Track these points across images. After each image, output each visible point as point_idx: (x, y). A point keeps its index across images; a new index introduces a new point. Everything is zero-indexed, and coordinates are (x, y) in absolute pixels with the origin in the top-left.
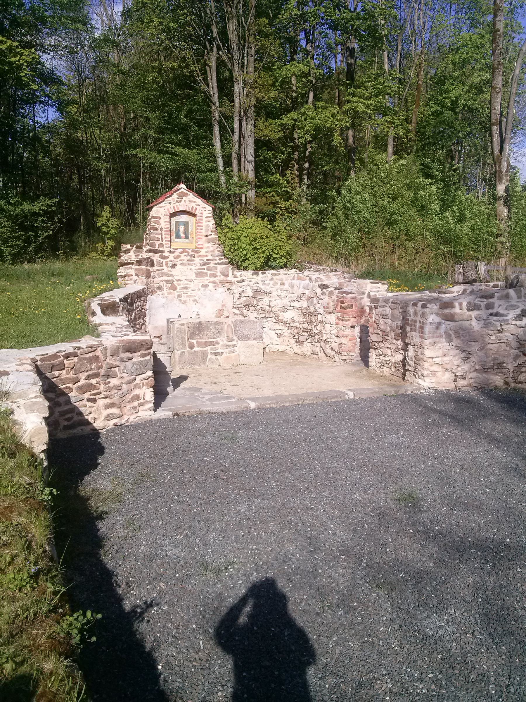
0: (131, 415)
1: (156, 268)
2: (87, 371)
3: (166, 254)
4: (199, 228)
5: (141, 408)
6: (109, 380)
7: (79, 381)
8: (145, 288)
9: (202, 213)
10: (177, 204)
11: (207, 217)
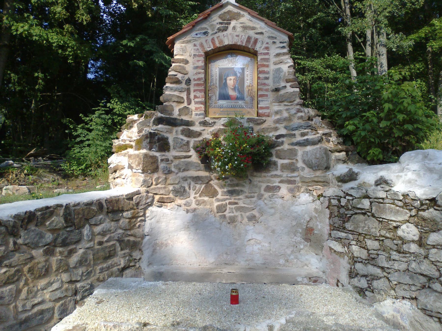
1: (173, 153)
3: (197, 128)
4: (261, 76)
8: (138, 193)
9: (267, 48)
10: (221, 34)
11: (278, 55)
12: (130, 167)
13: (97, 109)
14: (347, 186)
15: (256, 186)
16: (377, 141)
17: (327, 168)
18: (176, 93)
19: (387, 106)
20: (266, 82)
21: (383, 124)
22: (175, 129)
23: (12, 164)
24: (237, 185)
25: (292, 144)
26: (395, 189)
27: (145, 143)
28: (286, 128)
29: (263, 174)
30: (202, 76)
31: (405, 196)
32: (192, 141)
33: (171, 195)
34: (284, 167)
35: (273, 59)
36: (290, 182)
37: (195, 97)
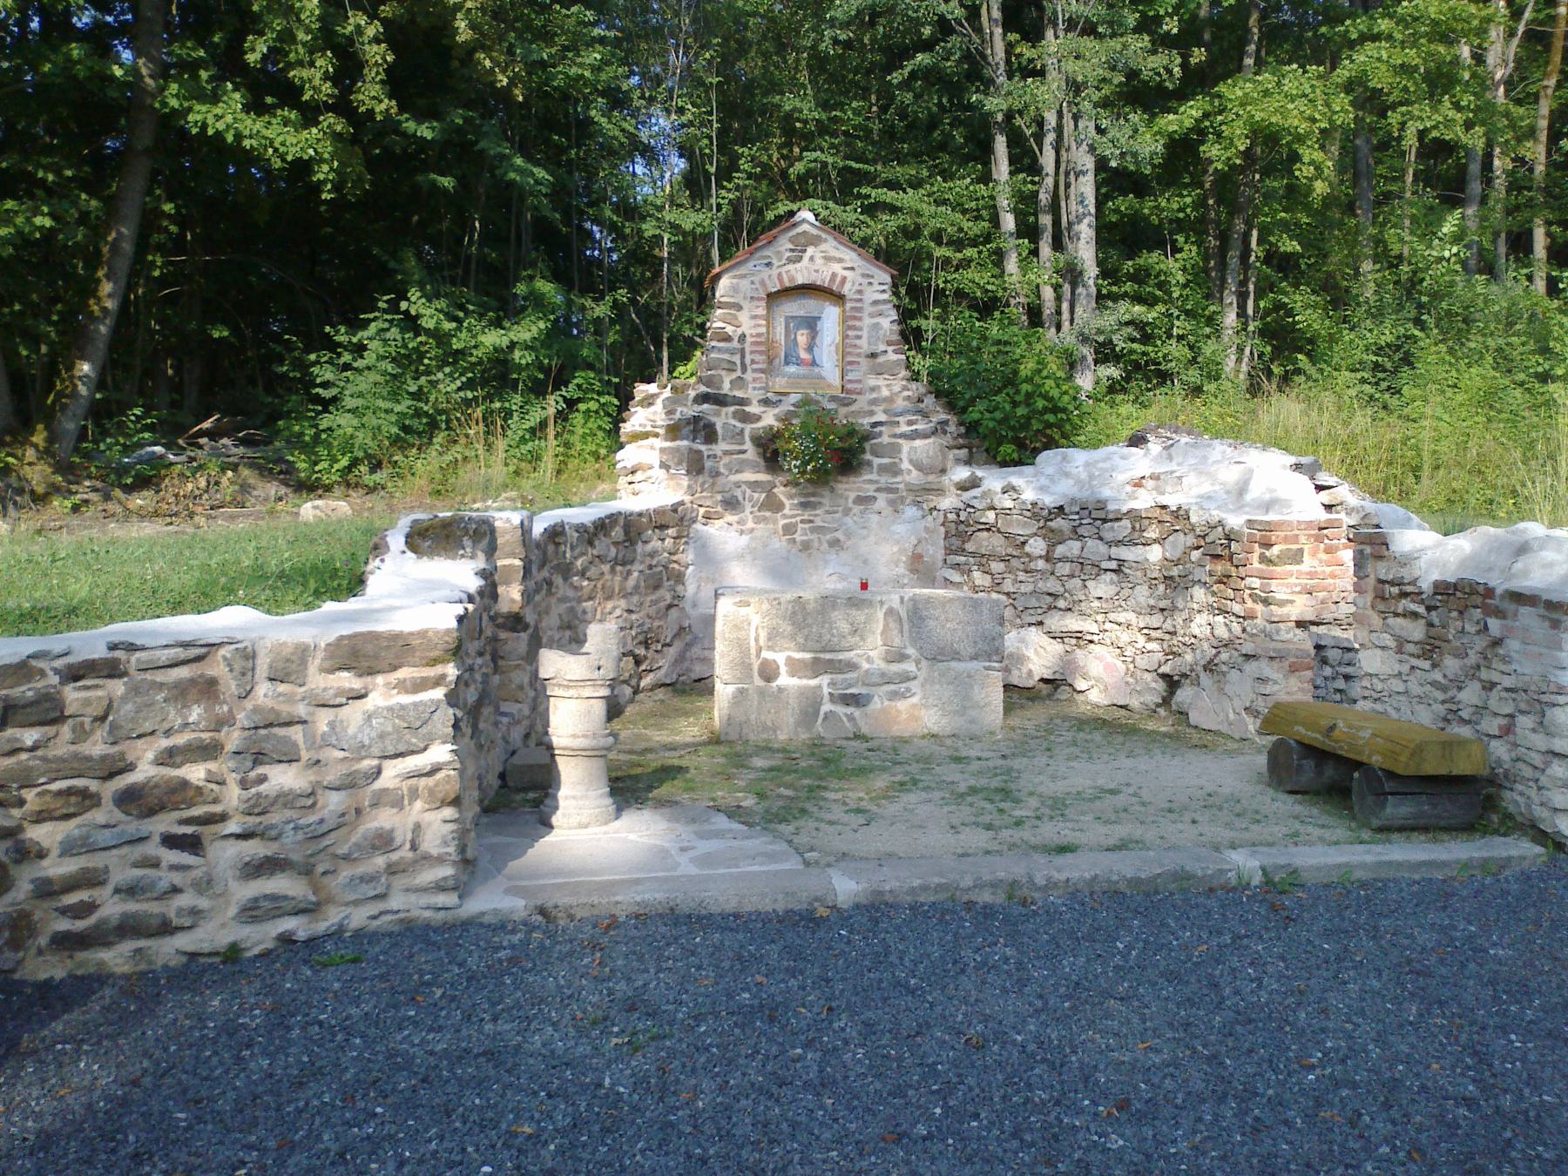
0: (356, 903)
1: (721, 446)
2: (168, 733)
3: (754, 409)
4: (850, 333)
5: (400, 882)
6: (261, 770)
7: (130, 768)
8: (682, 503)
9: (860, 292)
10: (791, 267)
11: (876, 303)
12: (664, 466)
13: (371, 316)
14: (967, 495)
15: (841, 496)
16: (1010, 434)
17: (943, 471)
18: (726, 356)
19: (1025, 387)
20: (857, 342)
21: (1021, 411)
22: (725, 410)
23: (162, 457)
24: (813, 495)
25: (895, 436)
26: (1023, 497)
27: (686, 430)
28: (885, 412)
29: (852, 479)
30: (763, 330)
31: (1034, 504)
32: (748, 428)
33: (719, 509)
34: (883, 469)
35: (869, 309)
36: (889, 490)
37: (753, 362)
